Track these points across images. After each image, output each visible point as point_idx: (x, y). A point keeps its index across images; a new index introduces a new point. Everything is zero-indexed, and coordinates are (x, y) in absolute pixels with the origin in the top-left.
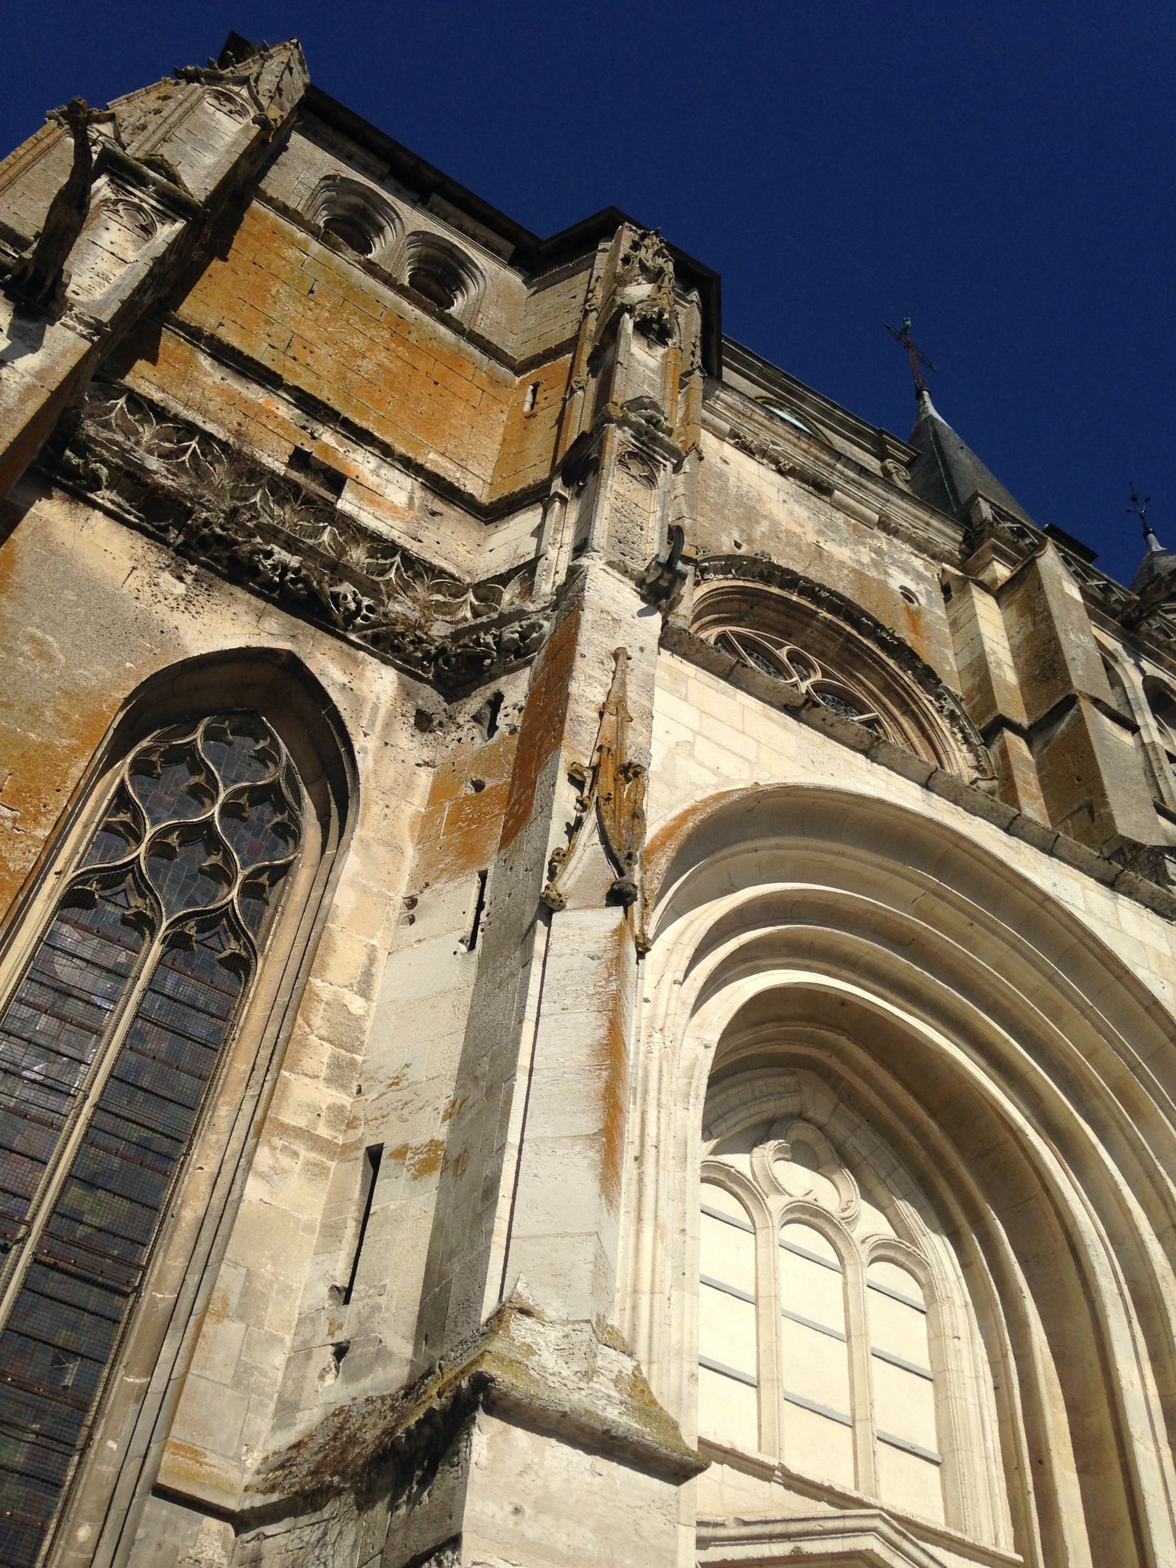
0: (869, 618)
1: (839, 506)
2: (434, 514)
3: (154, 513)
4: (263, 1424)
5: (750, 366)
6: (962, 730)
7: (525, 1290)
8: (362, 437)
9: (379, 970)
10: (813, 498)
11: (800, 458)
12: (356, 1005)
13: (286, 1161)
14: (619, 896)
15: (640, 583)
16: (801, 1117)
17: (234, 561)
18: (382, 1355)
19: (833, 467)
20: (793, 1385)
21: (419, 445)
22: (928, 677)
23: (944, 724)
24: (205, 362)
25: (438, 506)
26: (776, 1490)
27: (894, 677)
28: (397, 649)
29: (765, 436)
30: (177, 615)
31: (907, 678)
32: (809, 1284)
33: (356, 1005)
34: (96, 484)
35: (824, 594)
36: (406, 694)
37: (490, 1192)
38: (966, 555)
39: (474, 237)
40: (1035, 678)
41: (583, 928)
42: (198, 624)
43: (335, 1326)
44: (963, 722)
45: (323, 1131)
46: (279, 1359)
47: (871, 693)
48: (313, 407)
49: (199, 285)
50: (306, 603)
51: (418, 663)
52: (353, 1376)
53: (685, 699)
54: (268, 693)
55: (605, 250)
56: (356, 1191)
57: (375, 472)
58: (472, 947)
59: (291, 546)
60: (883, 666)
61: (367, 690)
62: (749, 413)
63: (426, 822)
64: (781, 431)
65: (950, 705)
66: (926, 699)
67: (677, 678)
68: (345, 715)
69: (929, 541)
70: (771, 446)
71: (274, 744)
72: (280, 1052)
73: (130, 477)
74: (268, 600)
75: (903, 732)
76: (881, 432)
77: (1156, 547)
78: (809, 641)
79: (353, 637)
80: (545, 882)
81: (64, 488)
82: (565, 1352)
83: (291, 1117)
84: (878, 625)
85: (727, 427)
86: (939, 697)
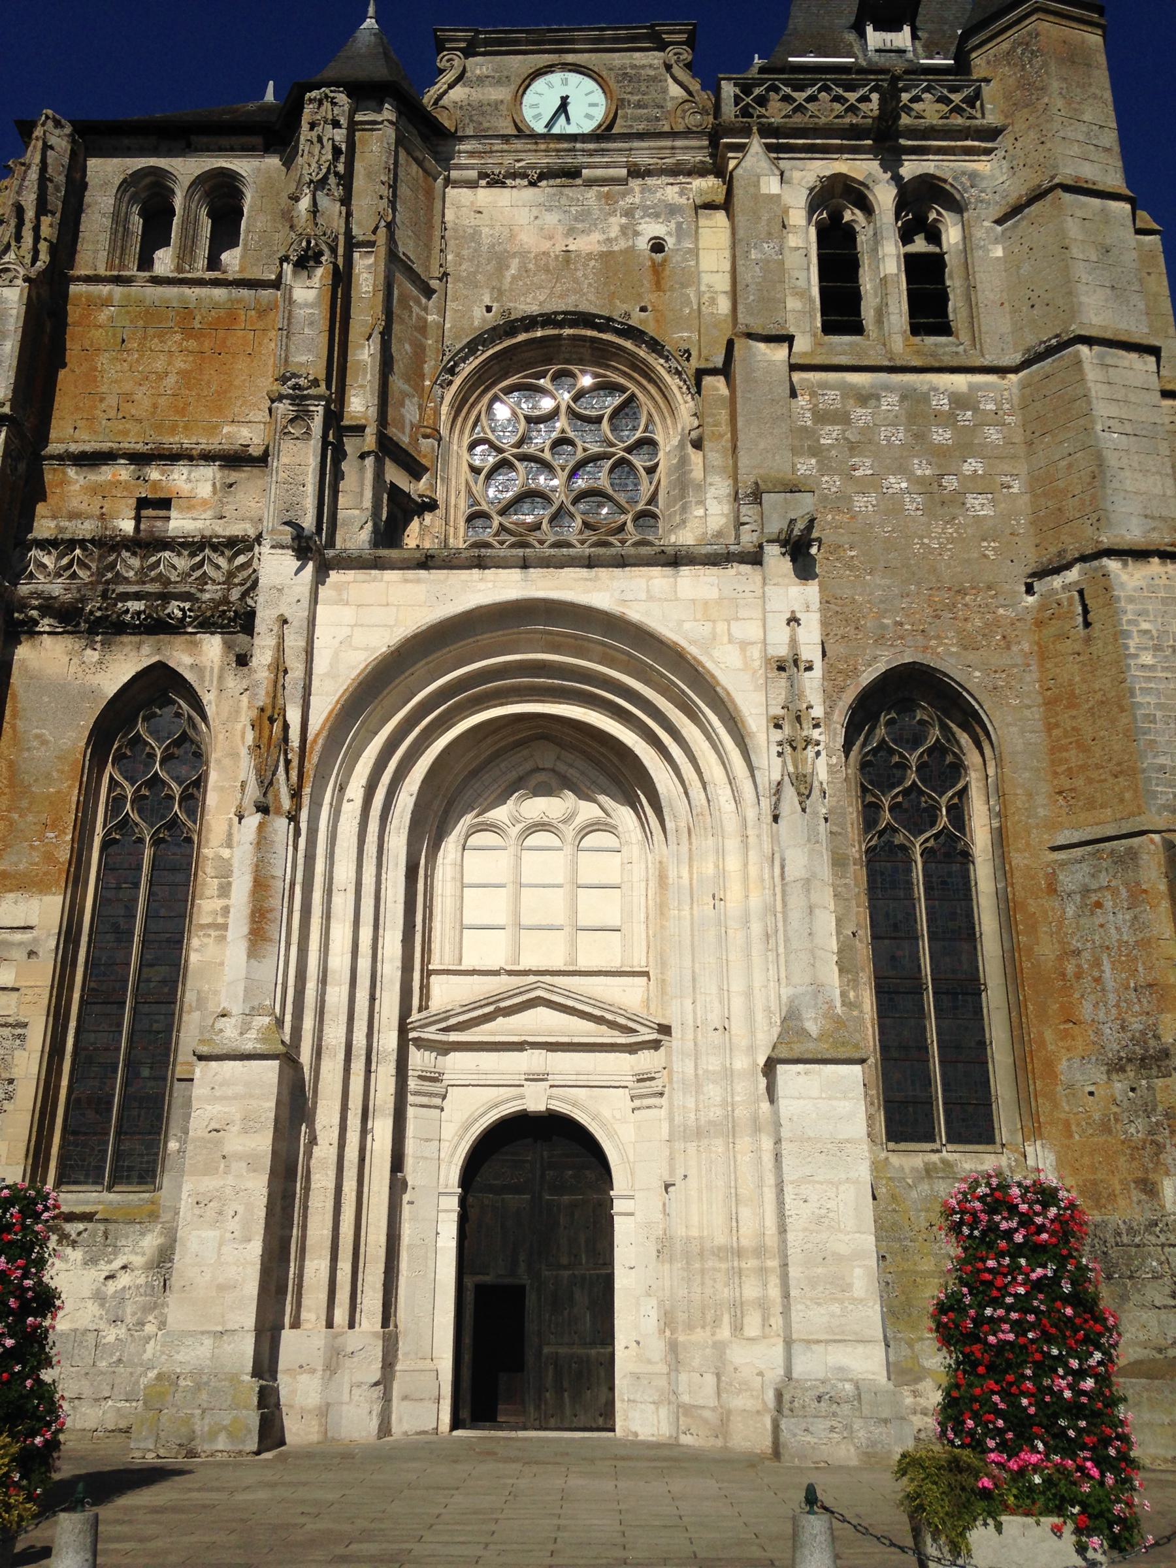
0: (600, 317)
1: (590, 183)
2: (231, 486)
3: (70, 618)
5: (517, 42)
8: (173, 457)
10: (566, 191)
11: (544, 160)
13: (206, 940)
16: (537, 770)
17: (113, 624)
19: (574, 150)
21: (214, 429)
23: (673, 382)
24: (71, 472)
25: (234, 476)
28: (214, 624)
29: (508, 160)
30: (98, 676)
32: (546, 862)
34: (36, 623)
35: (560, 317)
39: (232, 150)
42: (109, 675)
47: (625, 374)
48: (140, 459)
49: (56, 406)
50: (157, 626)
53: (347, 604)
54: (161, 687)
55: (311, 100)
57: (189, 480)
59: (137, 596)
62: (488, 148)
66: (658, 364)
68: (195, 685)
70: (518, 165)
71: (180, 707)
73: (49, 607)
74: (141, 634)
75: (653, 398)
76: (652, 26)
78: (567, 356)
79: (190, 630)
81: (25, 633)
84: (609, 319)
85: (473, 174)
86: (667, 359)
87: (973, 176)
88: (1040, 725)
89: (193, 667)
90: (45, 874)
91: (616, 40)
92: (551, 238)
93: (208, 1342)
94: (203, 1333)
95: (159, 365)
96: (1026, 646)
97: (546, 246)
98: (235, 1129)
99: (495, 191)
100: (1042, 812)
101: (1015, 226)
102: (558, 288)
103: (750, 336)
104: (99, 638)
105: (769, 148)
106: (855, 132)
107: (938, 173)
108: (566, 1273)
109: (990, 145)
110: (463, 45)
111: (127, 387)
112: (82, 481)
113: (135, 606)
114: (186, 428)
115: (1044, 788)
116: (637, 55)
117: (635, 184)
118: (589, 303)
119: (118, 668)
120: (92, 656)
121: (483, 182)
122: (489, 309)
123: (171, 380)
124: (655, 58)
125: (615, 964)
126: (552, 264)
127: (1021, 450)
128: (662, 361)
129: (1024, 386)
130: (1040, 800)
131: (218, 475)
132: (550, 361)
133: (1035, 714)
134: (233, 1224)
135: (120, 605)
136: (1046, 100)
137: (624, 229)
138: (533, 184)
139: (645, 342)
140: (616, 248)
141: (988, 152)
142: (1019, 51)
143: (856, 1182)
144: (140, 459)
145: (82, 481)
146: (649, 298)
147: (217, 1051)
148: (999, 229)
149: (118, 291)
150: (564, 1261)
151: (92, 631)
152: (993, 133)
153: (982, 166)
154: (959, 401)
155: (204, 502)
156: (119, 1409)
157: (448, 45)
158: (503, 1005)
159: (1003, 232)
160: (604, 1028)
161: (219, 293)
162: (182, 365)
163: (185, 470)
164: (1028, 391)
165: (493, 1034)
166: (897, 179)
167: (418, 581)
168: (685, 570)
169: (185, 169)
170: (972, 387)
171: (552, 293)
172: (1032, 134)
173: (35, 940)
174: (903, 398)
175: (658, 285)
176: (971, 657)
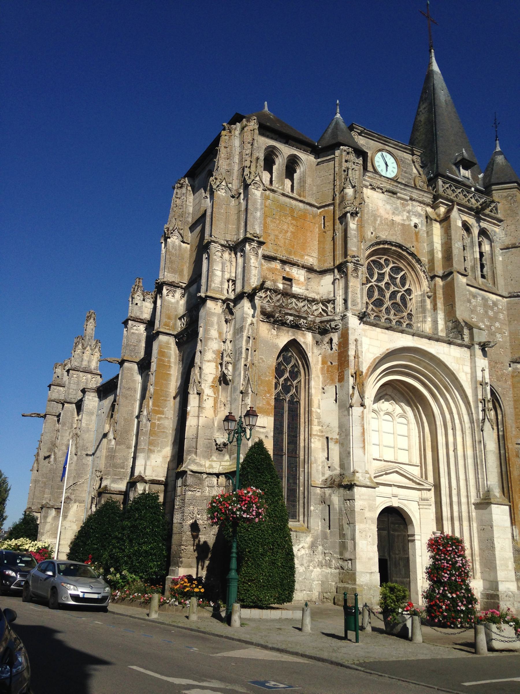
0: (405, 247)
1: (399, 198)
4: (321, 476)
5: (374, 137)
6: (426, 275)
7: (357, 469)
8: (294, 264)
9: (320, 403)
10: (392, 198)
12: (318, 411)
13: (315, 440)
14: (362, 405)
15: (358, 316)
16: (386, 394)
18: (335, 469)
20: (385, 444)
21: (302, 256)
22: (419, 261)
23: (422, 274)
26: (383, 462)
27: (411, 262)
29: (379, 183)
31: (414, 261)
33: (318, 411)
35: (394, 244)
36: (314, 337)
37: (349, 453)
38: (434, 202)
40: (445, 258)
41: (356, 411)
43: (328, 464)
44: (426, 274)
45: (319, 434)
46: (320, 467)
48: (284, 262)
50: (296, 327)
51: (315, 331)
52: (332, 471)
56: (326, 444)
58: (336, 402)
59: (291, 315)
60: (408, 258)
61: (307, 339)
62: (374, 177)
63: (322, 369)
64: (383, 180)
65: (423, 269)
66: (418, 266)
67: (364, 330)
69: (423, 200)
72: (309, 422)
75: (412, 276)
77: (498, 149)
79: (303, 329)
80: (350, 400)
82: (363, 477)
83: (314, 433)
86: (421, 266)
87: (495, 232)
88: (513, 407)
89: (304, 343)
90: (268, 409)
91: (400, 147)
92: (388, 214)
93: (368, 575)
94: (367, 572)
95: (285, 227)
96: (510, 383)
97: (387, 216)
98: (367, 510)
99: (372, 191)
100: (514, 433)
101: (506, 252)
102: (391, 232)
103: (458, 272)
104: (276, 326)
105: (459, 210)
106: (471, 209)
107: (488, 229)
108: (397, 556)
109: (499, 224)
110: (359, 131)
111: (277, 233)
112: (266, 266)
113: (291, 318)
114: (294, 253)
115: (514, 426)
116: (405, 154)
117: (410, 202)
118: (400, 241)
119: (283, 338)
120: (274, 332)
121: (370, 187)
122: (372, 233)
123: (289, 234)
124: (409, 157)
125: (393, 460)
126: (389, 224)
127: (507, 323)
128: (419, 266)
129: (508, 303)
130: (513, 429)
131: (306, 274)
132: (384, 255)
133: (512, 403)
134: (370, 539)
135: (286, 317)
136: (518, 218)
137: (408, 217)
138: (383, 193)
139: (415, 258)
140: (406, 223)
141: (499, 226)
142: (510, 198)
143: (509, 539)
144: (284, 262)
145: (266, 266)
146: (415, 244)
147: (362, 484)
148: (501, 251)
149: (272, 194)
150: (397, 552)
151: (275, 322)
152: (500, 221)
153: (497, 229)
154: (495, 304)
155: (302, 283)
156: (308, 594)
157: (355, 130)
158: (387, 472)
159: (502, 253)
160: (411, 482)
161: (301, 205)
162: (293, 230)
163: (296, 269)
164: (509, 305)
165: (381, 480)
166: (479, 226)
167: (385, 333)
168: (452, 346)
169: (286, 151)
170: (497, 300)
171: (389, 234)
172: (513, 226)
173: (267, 432)
174: (482, 299)
175: (417, 240)
176: (499, 383)
